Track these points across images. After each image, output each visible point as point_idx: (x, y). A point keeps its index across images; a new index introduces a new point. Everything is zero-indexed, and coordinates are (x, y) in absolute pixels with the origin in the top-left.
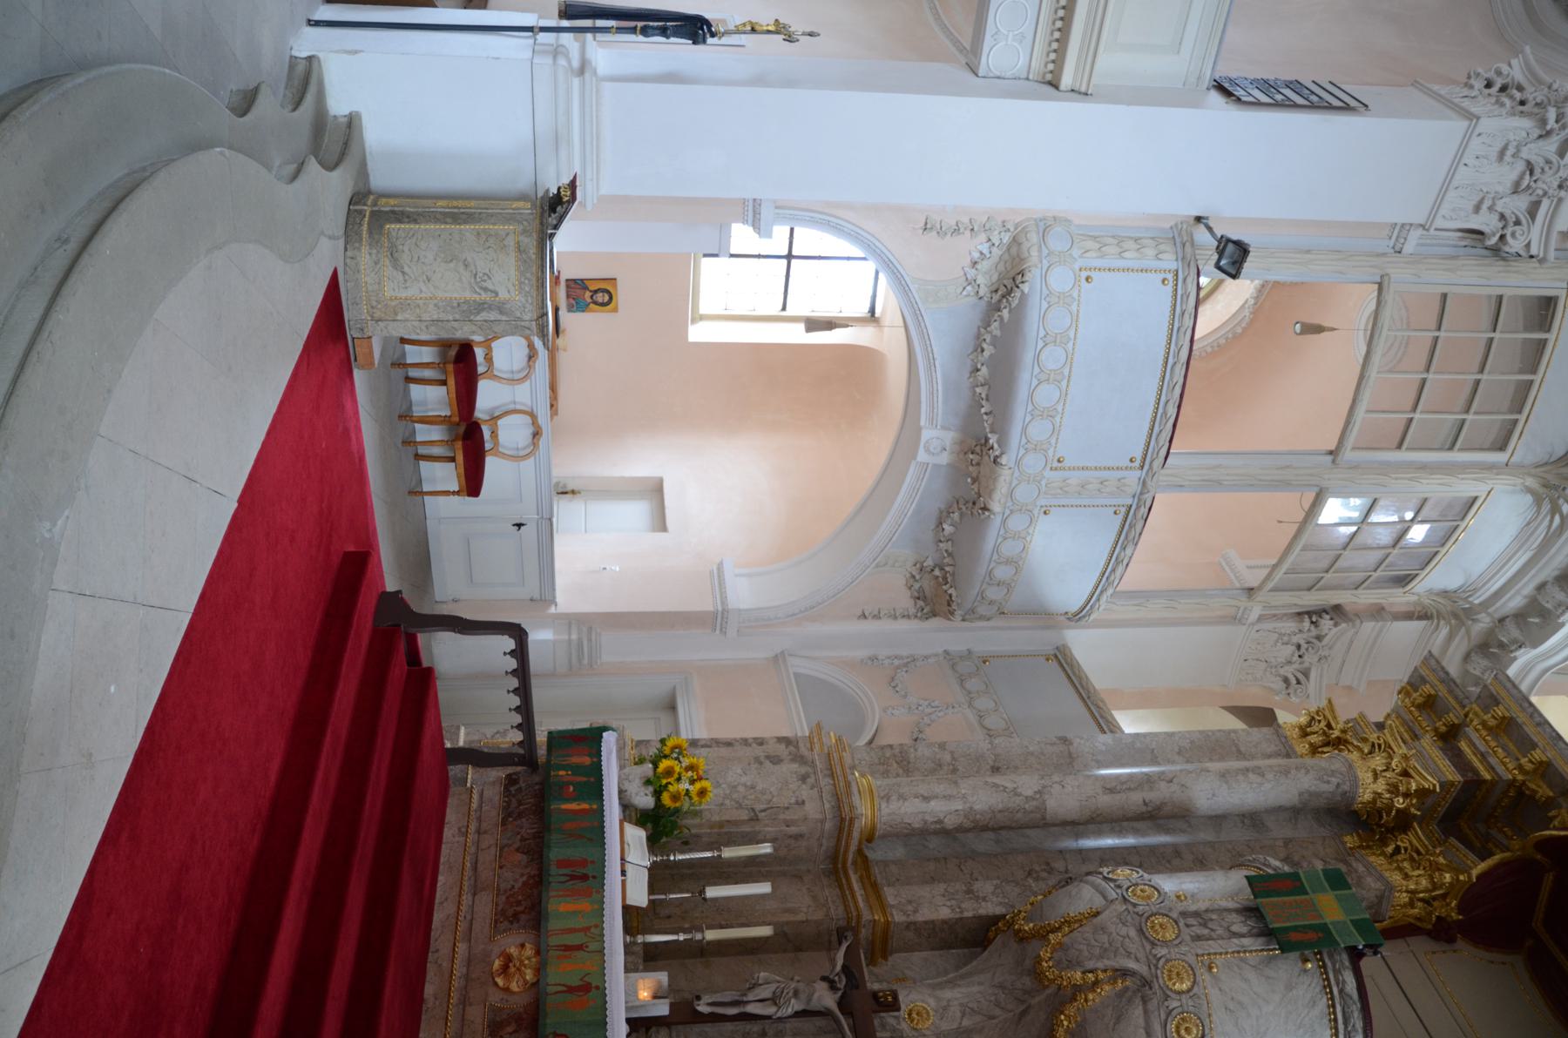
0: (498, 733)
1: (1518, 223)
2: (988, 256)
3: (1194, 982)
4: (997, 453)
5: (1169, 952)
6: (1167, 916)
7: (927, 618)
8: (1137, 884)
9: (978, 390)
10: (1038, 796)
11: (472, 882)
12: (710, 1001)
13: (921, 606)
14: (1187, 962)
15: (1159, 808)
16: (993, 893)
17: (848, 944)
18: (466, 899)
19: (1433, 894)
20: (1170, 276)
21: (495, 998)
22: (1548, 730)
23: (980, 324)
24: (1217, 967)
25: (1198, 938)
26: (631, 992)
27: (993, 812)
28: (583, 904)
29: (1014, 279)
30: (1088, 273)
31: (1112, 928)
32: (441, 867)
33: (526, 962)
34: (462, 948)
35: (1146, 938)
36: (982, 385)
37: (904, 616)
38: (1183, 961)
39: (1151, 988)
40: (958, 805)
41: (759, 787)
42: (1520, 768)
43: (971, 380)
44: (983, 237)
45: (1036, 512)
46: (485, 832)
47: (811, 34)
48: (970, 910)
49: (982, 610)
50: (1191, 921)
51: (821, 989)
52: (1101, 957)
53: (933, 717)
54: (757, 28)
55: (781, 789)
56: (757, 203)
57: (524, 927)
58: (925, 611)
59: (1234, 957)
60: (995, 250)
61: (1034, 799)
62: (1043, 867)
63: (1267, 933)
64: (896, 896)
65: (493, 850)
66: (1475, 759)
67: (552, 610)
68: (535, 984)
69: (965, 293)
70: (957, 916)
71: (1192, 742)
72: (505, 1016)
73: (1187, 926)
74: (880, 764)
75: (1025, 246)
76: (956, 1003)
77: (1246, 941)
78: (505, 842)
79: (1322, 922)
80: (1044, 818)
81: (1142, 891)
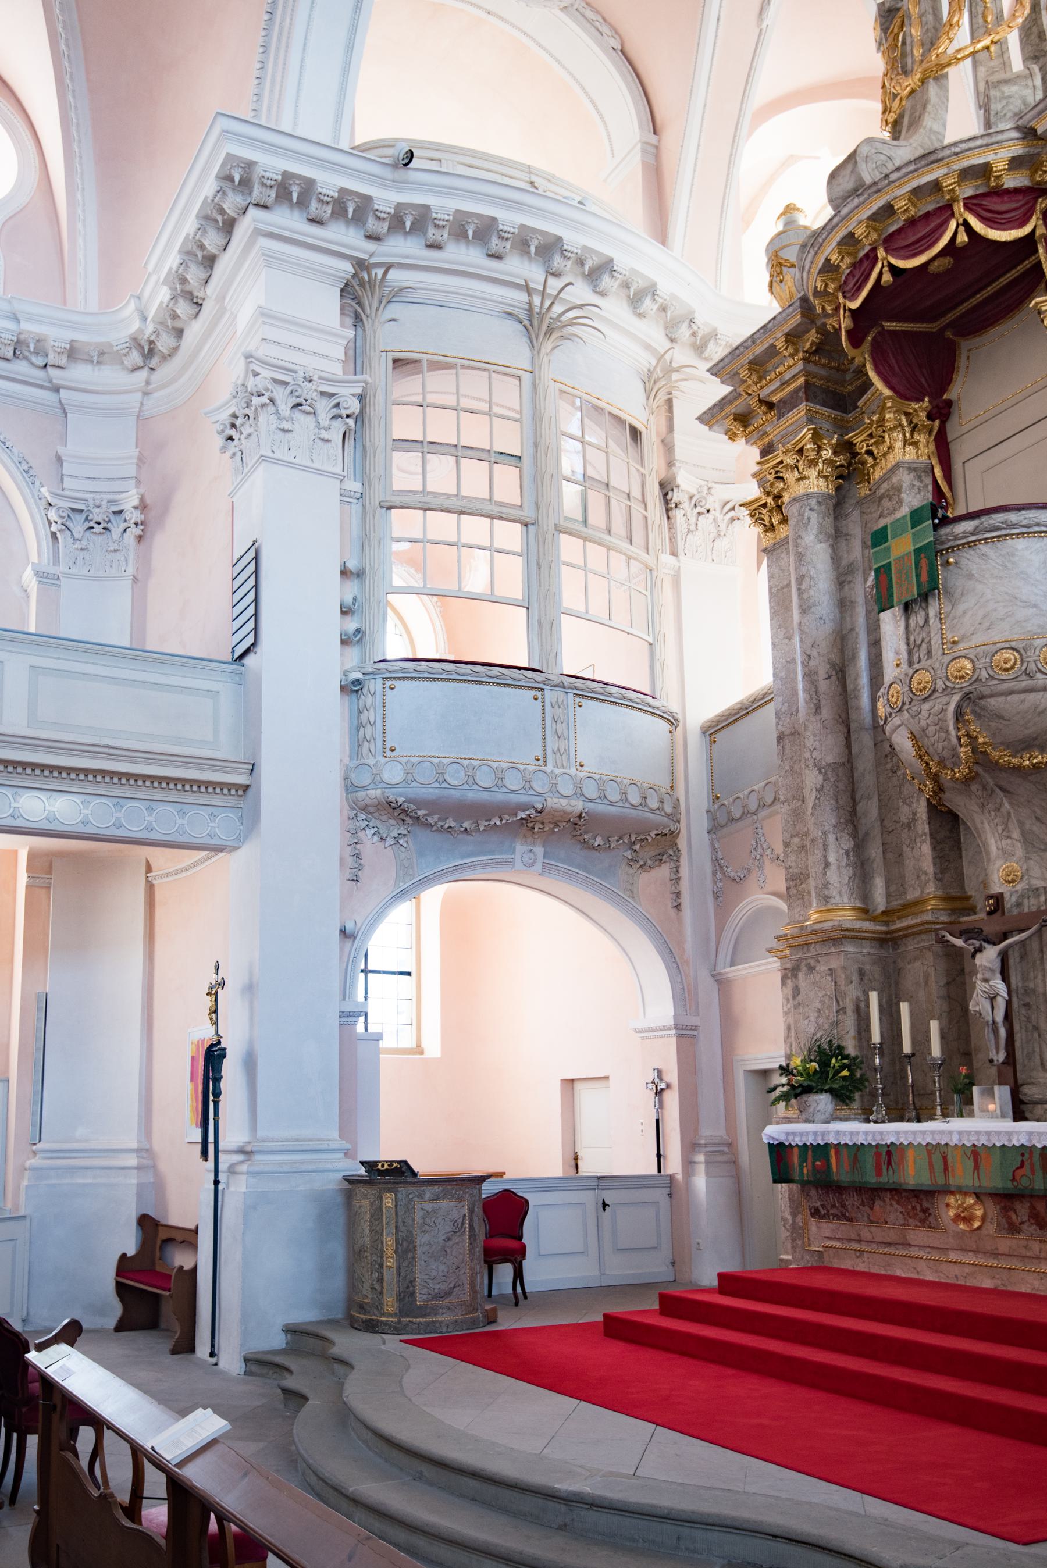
0: (784, 1226)
1: (337, 405)
2: (376, 829)
3: (965, 657)
4: (533, 811)
5: (941, 678)
6: (912, 678)
7: (679, 851)
8: (888, 699)
9: (482, 828)
10: (823, 770)
11: (901, 1247)
12: (994, 1051)
13: (668, 857)
14: (949, 663)
15: (833, 665)
16: (910, 806)
17: (948, 935)
18: (914, 1252)
19: (906, 424)
20: (388, 683)
21: (991, 1228)
22: (758, 335)
23: (428, 831)
24: (953, 637)
25: (929, 653)
26: (993, 1116)
27: (837, 808)
28: (910, 1155)
29: (394, 809)
30: (388, 750)
31: (923, 723)
32: (889, 1273)
33: (959, 1202)
34: (953, 1256)
35: (930, 696)
36: (478, 826)
37: (677, 871)
38: (948, 667)
39: (971, 693)
40: (831, 838)
41: (818, 1005)
42: (792, 356)
43: (474, 834)
44: (361, 834)
45: (581, 775)
46: (859, 1235)
47: (217, 967)
48: (923, 827)
49: (669, 809)
50: (915, 658)
51: (981, 960)
52: (947, 732)
53: (765, 846)
54: (214, 1009)
55: (820, 987)
56: (343, 1015)
57: (933, 1204)
58: (672, 853)
59: (945, 623)
60: (371, 824)
61: (826, 773)
62: (889, 760)
63: (924, 597)
64: (914, 889)
65: (873, 1229)
66: (787, 389)
67: (679, 1177)
68: (977, 1195)
69: (405, 845)
70: (928, 838)
71: (780, 627)
72: (1004, 1221)
73: (919, 661)
74: (803, 899)
75: (368, 801)
76: (999, 843)
77: (932, 612)
78: (866, 1219)
79: (913, 553)
80: (843, 764)
81: (893, 697)
